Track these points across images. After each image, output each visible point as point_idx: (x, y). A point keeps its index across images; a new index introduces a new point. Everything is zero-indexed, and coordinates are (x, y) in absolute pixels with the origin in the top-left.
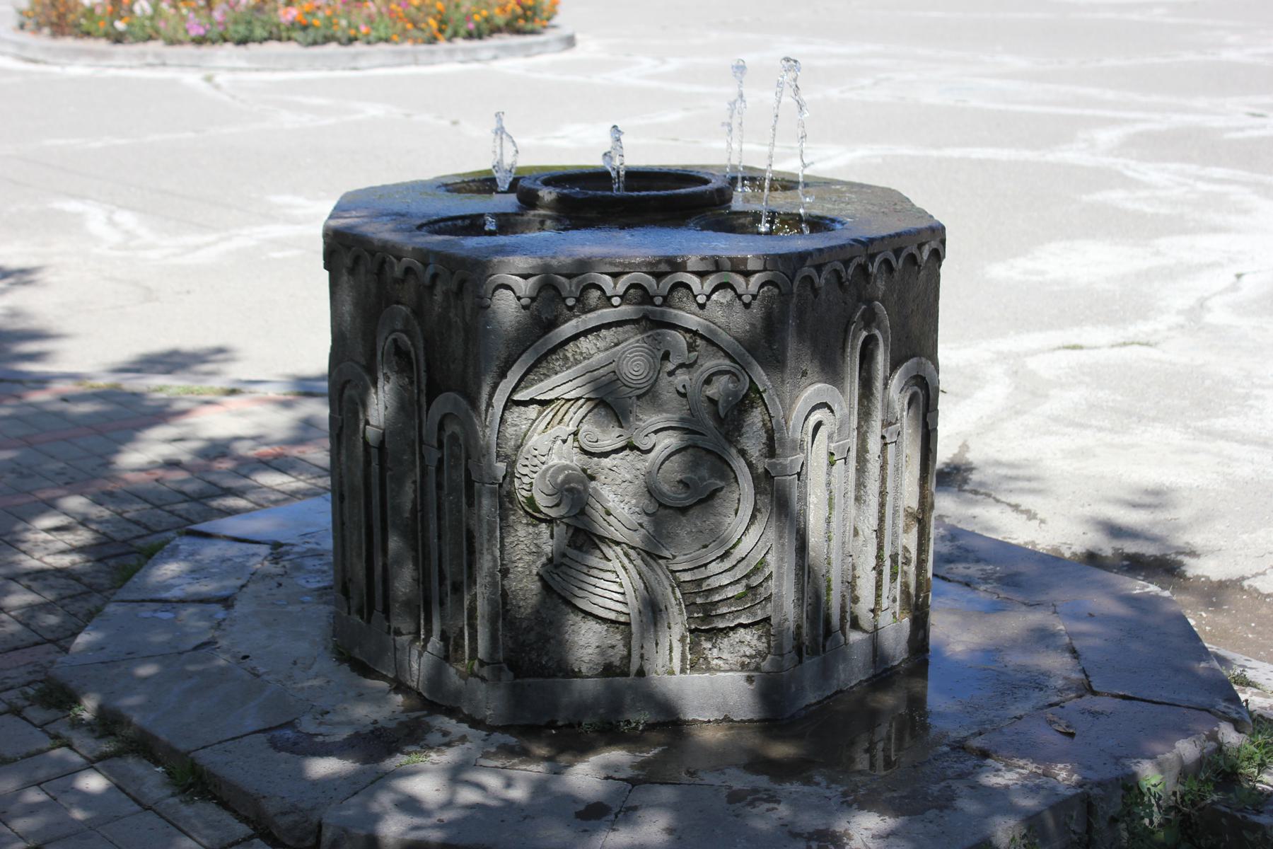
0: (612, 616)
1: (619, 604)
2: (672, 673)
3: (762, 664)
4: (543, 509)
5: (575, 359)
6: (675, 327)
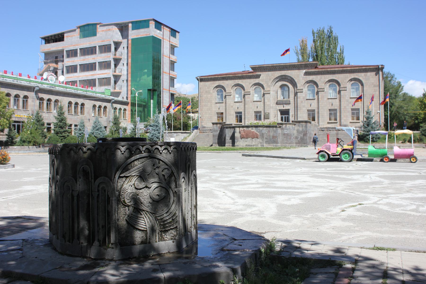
0: (143, 229)
2: (156, 242)
5: (134, 166)
6: (155, 158)
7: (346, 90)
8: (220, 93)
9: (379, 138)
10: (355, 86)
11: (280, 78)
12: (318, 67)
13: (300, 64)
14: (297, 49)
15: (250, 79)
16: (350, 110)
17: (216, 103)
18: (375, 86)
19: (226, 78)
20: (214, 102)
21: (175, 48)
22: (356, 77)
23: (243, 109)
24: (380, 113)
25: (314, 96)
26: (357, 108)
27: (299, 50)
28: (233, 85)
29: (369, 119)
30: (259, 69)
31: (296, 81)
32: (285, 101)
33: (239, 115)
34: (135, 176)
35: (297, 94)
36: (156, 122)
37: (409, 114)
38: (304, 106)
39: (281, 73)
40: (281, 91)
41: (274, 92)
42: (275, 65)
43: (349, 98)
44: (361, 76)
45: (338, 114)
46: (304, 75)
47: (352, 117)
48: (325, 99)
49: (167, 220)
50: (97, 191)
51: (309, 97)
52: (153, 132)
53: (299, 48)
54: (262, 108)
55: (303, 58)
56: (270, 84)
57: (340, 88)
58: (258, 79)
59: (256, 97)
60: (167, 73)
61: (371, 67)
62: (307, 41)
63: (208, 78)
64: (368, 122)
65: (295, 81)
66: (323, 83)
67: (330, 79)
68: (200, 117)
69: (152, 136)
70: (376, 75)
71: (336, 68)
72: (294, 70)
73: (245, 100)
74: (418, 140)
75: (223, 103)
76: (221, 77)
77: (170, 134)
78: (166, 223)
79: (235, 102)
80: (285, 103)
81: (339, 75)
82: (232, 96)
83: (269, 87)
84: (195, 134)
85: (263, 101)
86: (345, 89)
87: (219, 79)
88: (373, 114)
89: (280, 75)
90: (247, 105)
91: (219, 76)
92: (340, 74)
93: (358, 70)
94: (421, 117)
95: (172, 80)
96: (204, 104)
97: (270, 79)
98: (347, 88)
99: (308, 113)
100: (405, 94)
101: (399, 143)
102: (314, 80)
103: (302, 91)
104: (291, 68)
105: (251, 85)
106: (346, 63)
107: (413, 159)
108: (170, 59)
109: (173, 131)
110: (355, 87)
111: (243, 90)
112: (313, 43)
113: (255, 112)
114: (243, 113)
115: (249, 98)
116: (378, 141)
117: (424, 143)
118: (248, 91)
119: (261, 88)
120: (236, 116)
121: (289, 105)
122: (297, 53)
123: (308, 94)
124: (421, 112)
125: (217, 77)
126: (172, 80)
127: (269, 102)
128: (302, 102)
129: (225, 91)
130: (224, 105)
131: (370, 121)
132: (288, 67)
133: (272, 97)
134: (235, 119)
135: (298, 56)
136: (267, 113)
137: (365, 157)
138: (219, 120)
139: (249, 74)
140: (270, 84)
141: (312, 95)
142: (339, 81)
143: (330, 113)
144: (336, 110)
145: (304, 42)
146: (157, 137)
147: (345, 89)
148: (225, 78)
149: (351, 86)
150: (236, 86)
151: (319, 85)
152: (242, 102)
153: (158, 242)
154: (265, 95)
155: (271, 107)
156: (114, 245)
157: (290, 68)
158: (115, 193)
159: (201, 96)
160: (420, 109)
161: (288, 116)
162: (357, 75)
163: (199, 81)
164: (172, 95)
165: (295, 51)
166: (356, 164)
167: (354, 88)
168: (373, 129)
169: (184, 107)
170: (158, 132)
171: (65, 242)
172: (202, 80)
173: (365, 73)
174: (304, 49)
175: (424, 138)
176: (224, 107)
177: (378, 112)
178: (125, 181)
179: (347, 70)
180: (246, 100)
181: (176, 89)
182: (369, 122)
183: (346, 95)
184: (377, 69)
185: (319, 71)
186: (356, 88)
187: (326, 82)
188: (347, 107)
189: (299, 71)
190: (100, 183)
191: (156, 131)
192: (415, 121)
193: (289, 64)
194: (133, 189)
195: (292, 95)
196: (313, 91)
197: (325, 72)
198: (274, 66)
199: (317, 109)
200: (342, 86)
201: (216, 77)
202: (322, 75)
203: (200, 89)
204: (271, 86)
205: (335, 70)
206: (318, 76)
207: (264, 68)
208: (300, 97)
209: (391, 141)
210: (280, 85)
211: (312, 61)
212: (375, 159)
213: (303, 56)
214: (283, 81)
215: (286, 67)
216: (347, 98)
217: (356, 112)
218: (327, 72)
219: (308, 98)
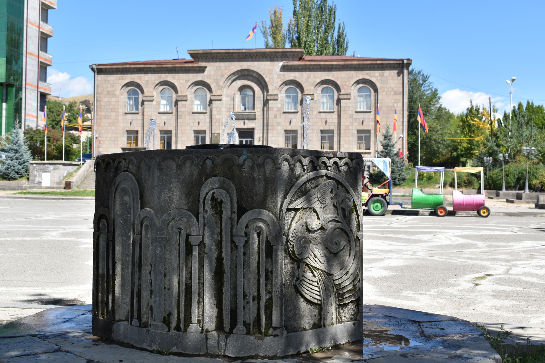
0: (316, 301)
1: (256, 311)
2: (333, 324)
3: (357, 317)
4: (297, 256)
7: (349, 99)
8: (133, 95)
9: (404, 179)
10: (364, 93)
11: (240, 74)
12: (304, 59)
13: (275, 52)
14: (265, 26)
15: (188, 74)
16: (356, 132)
17: (126, 114)
18: (396, 93)
19: (145, 70)
20: (121, 111)
21: (50, 11)
22: (367, 77)
23: (174, 125)
24: (403, 138)
25: (296, 108)
26: (366, 128)
27: (268, 27)
28: (157, 82)
29: (389, 148)
30: (204, 56)
31: (267, 80)
32: (247, 115)
33: (166, 135)
34: (307, 208)
35: (268, 103)
36: (15, 144)
37: (445, 141)
38: (279, 124)
39: (241, 66)
40: (240, 96)
41: (229, 99)
42: (231, 51)
43: (354, 113)
44: (374, 76)
45: (335, 139)
46: (281, 71)
47: (358, 143)
48: (315, 113)
49: (347, 286)
50: (243, 234)
51: (288, 109)
52: (9, 161)
53: (269, 24)
54: (208, 124)
55: (275, 42)
56: (221, 84)
57: (339, 95)
58: (201, 74)
59: (197, 106)
60: (35, 55)
61: (391, 62)
62: (282, 13)
63: (113, 68)
64: (386, 152)
65: (265, 81)
66: (312, 86)
67: (323, 78)
68: (96, 138)
69: (8, 169)
70: (399, 75)
71: (334, 60)
72: (263, 61)
73: (177, 111)
74: (465, 183)
75: (138, 113)
76: (135, 68)
77: (42, 167)
78: (345, 291)
79: (159, 113)
80: (246, 117)
81: (338, 72)
82: (154, 103)
83: (221, 88)
84: (88, 167)
85: (208, 113)
86: (348, 97)
87: (131, 70)
88: (395, 139)
89: (239, 68)
90: (181, 118)
91: (133, 66)
92: (340, 71)
93: (370, 66)
94: (463, 147)
95: (43, 68)
96: (103, 114)
97: (222, 76)
98: (352, 94)
99: (286, 136)
100: (440, 109)
101: (436, 188)
102: (297, 79)
103: (276, 97)
104: (259, 58)
105: (189, 84)
106: (349, 54)
107: (484, 211)
108: (41, 30)
109: (46, 161)
110: (364, 94)
111: (174, 93)
112: (292, 18)
113: (194, 131)
114: (174, 132)
115: (185, 107)
116: (402, 185)
117: (474, 188)
118: (184, 94)
119: (207, 90)
120: (161, 137)
121: (254, 121)
122: (264, 33)
123: (286, 102)
124: (462, 138)
125: (128, 66)
126: (43, 68)
127: (220, 115)
128: (276, 116)
129: (143, 92)
130: (139, 117)
131: (390, 150)
132: (253, 55)
133: (224, 105)
134: (159, 143)
135: (266, 37)
136: (216, 135)
137: (406, 208)
138: (130, 143)
139: (186, 65)
140: (221, 84)
141: (293, 104)
142: (339, 82)
143: (322, 137)
144: (332, 132)
145: (278, 14)
146: (16, 172)
147: (348, 97)
148: (143, 71)
149: (358, 93)
150: (162, 85)
151: (305, 88)
152: (172, 113)
153: (335, 325)
154: (213, 102)
155: (222, 123)
156: (278, 330)
157: (257, 57)
158: (281, 237)
159: (99, 99)
160: (462, 134)
161: (252, 139)
162: (367, 74)
163: (96, 73)
164: (43, 96)
165: (262, 29)
166: (398, 219)
167: (362, 96)
168: (394, 164)
169: (57, 120)
170: (19, 162)
171: (169, 330)
172: (100, 70)
173: (380, 72)
174: (276, 26)
175: (474, 180)
176: (140, 121)
177: (400, 137)
178: (294, 217)
179: (352, 64)
180: (179, 110)
181: (50, 86)
182: (389, 153)
183: (349, 107)
184: (401, 65)
185: (305, 65)
186: (365, 95)
187: (316, 83)
188: (351, 127)
189: (272, 63)
190: (250, 221)
191: (15, 161)
192: (452, 153)
193: (255, 51)
194: (304, 231)
195: (259, 105)
196: (295, 99)
197: (315, 67)
198: (229, 53)
199: (300, 128)
200: (343, 92)
201: (126, 68)
202: (310, 71)
203: (97, 87)
204: (224, 87)
205: (332, 65)
206: (303, 73)
207: (212, 56)
208: (273, 108)
209: (423, 184)
210: (239, 86)
211: (290, 47)
212: (421, 211)
213: (274, 38)
214: (244, 79)
215: (250, 55)
216: (351, 112)
217: (365, 136)
218: (319, 67)
219: (286, 110)
